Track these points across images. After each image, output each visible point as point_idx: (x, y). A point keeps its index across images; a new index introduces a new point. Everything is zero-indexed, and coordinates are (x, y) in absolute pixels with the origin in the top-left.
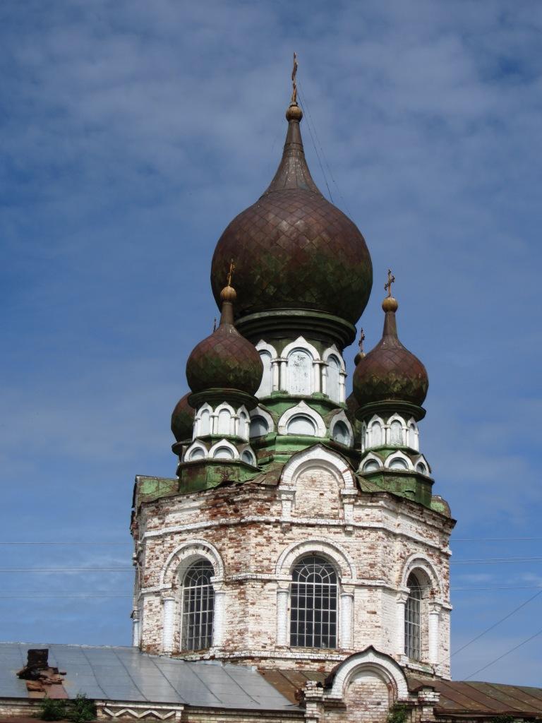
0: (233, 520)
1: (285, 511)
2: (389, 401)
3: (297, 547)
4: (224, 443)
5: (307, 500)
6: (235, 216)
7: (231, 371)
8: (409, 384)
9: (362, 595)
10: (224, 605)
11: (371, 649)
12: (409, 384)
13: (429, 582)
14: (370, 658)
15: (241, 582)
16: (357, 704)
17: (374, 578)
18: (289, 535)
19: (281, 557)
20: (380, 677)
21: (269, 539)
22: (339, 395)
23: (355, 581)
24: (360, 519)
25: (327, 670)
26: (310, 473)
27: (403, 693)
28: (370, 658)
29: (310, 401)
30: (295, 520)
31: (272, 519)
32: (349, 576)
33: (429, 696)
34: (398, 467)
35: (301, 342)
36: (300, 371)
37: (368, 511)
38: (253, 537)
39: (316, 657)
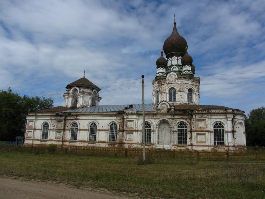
0: (161, 84)
1: (167, 82)
2: (185, 63)
3: (169, 87)
4: (160, 73)
5: (171, 80)
6: (165, 41)
7: (161, 63)
8: (188, 60)
9: (179, 93)
10: (160, 96)
11: (164, 101)
12: (188, 60)
13: (193, 90)
14: (164, 102)
15: (162, 93)
16: (162, 109)
17: (181, 90)
18: (168, 85)
19: (167, 89)
20: (166, 105)
21: (165, 86)
22: (180, 63)
23: (178, 91)
24: (179, 82)
25: (69, 107)
26: (171, 76)
27: (169, 107)
28: (164, 102)
29: (175, 65)
30: (169, 83)
31: (165, 83)
32: (177, 91)
33: (173, 107)
34: (187, 73)
35: (174, 57)
36: (174, 61)
37: (180, 80)
38: (163, 86)
39: (172, 103)
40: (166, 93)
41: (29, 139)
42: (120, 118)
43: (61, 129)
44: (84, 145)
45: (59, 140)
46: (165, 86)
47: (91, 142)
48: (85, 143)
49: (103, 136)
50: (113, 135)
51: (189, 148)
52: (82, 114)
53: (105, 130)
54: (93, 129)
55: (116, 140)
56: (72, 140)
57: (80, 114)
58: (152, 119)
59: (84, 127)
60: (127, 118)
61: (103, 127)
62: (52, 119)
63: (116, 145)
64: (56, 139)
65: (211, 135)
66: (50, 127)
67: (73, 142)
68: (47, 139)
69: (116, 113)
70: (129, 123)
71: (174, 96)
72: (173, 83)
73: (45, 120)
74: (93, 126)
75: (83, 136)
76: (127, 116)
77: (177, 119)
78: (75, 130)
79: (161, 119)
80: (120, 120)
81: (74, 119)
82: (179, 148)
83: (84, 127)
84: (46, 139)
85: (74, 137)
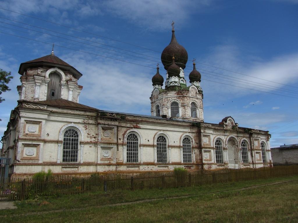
15: (184, 106)
40: (189, 107)
41: (33, 162)
42: (194, 131)
43: (114, 144)
44: (152, 169)
45: (110, 162)
46: (188, 99)
47: (160, 164)
48: (154, 166)
49: (175, 156)
50: (187, 153)
51: (251, 166)
52: (144, 120)
53: (57, 142)
54: (161, 144)
55: (191, 160)
56: (130, 163)
57: (140, 119)
58: (222, 135)
59: (148, 140)
60: (204, 132)
61: (174, 142)
62: (89, 124)
63: (192, 166)
64: (102, 162)
65: (124, 149)
66: (83, 137)
67: (134, 166)
68: (75, 163)
69: (188, 124)
70: (204, 138)
71: (173, 110)
72: (193, 97)
73: (71, 123)
74: (162, 139)
75: (147, 155)
76: (204, 130)
77: (240, 137)
78: (133, 145)
79: (230, 136)
80: (193, 134)
81: (132, 126)
82: (221, 167)
83: (148, 140)
84: (73, 163)
85: (132, 157)
